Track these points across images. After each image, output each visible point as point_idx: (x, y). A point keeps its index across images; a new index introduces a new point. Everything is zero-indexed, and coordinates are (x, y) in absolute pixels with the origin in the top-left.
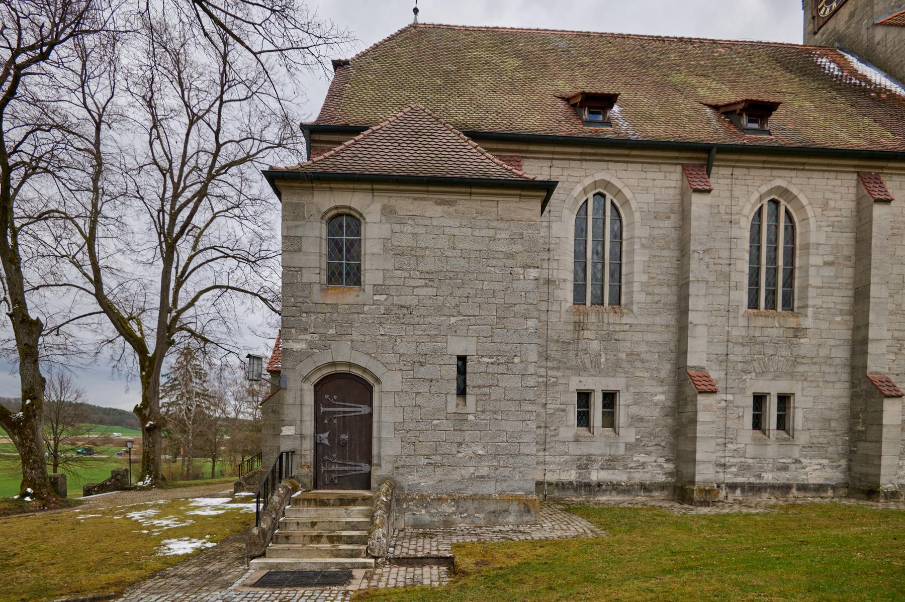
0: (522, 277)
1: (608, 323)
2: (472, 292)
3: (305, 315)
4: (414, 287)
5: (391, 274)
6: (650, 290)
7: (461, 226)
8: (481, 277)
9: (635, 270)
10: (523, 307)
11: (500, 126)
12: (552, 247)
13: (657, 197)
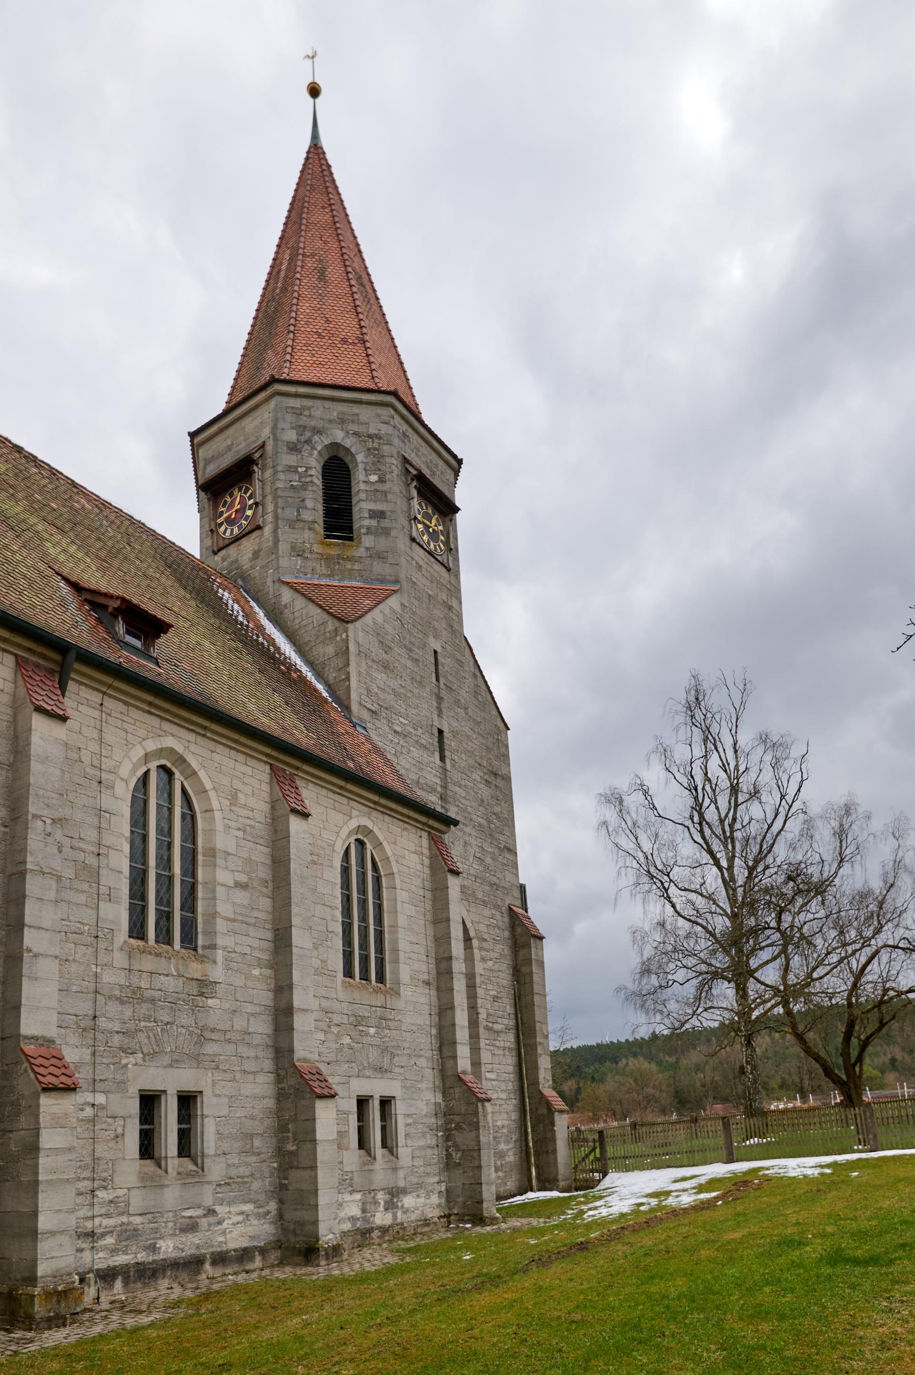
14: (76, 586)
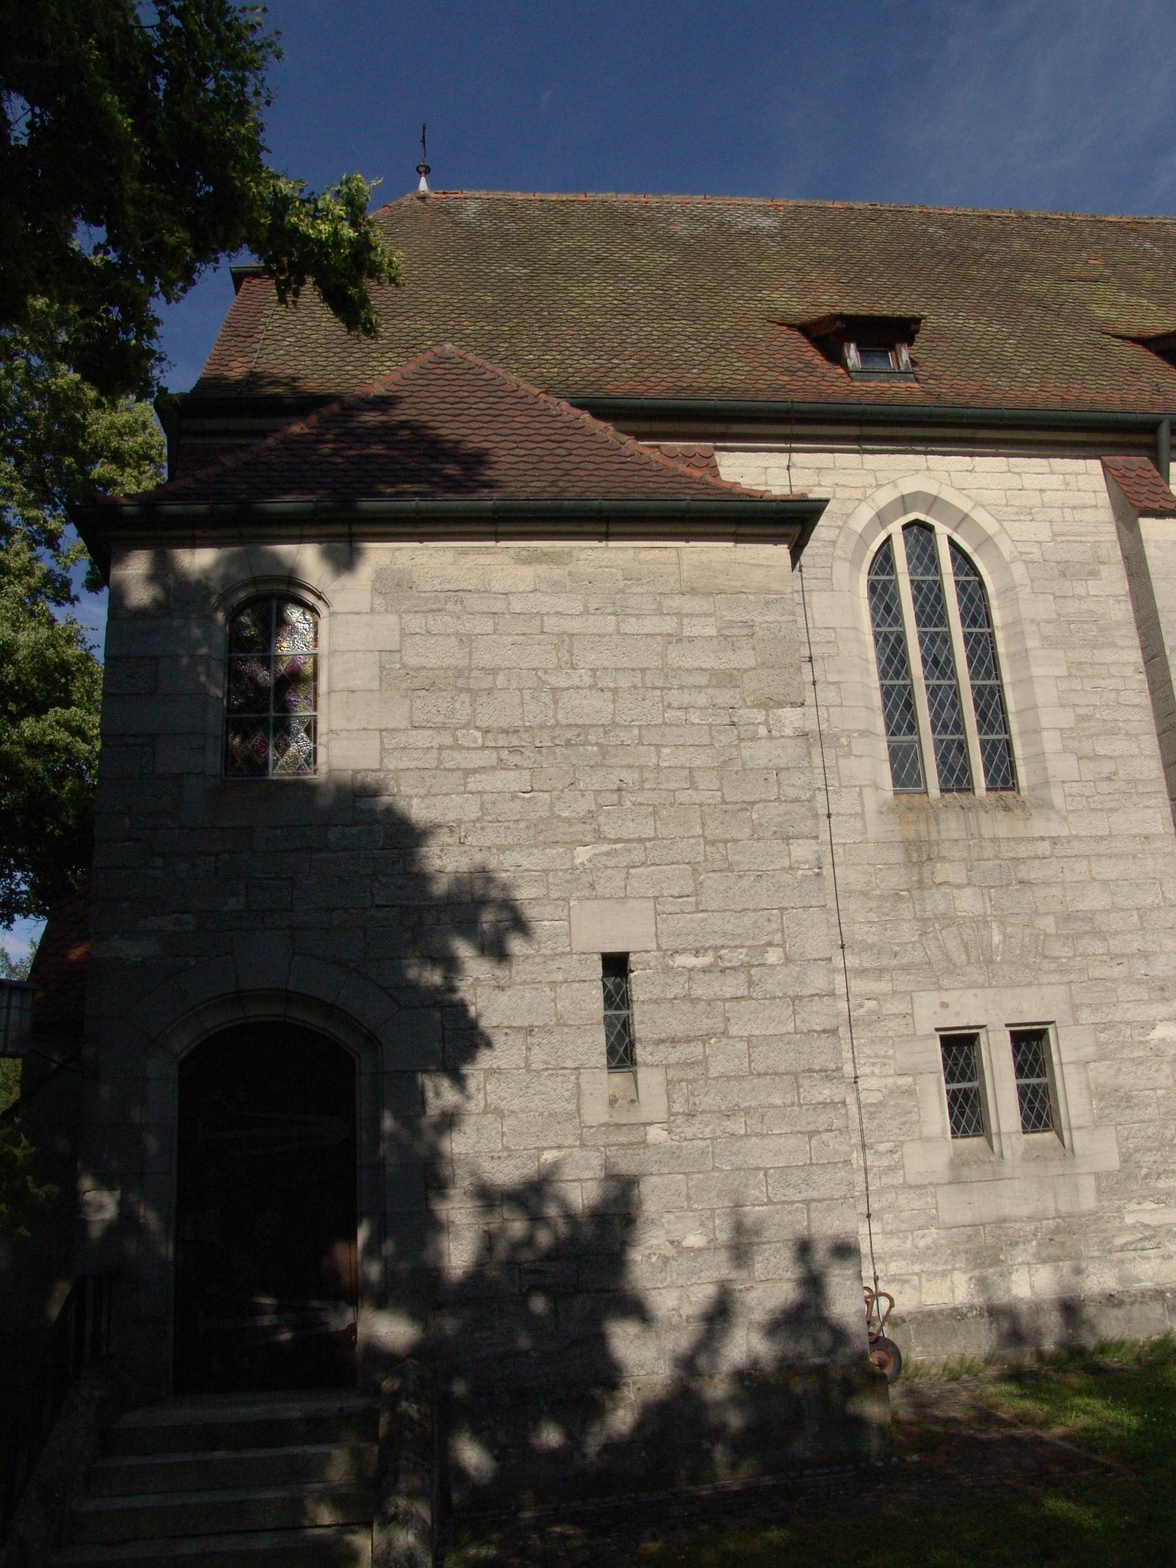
0: (762, 731)
1: (995, 840)
2: (631, 777)
3: (159, 862)
4: (469, 772)
5: (402, 739)
6: (1086, 747)
7: (586, 612)
8: (652, 737)
9: (1040, 700)
10: (774, 809)
11: (658, 386)
12: (816, 651)
13: (1056, 528)
14: (1139, 341)
